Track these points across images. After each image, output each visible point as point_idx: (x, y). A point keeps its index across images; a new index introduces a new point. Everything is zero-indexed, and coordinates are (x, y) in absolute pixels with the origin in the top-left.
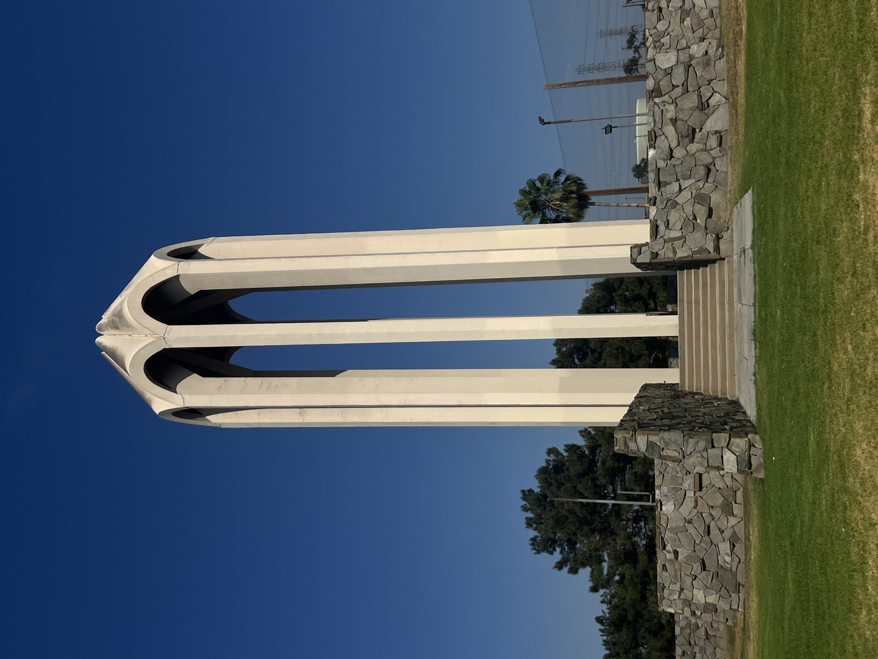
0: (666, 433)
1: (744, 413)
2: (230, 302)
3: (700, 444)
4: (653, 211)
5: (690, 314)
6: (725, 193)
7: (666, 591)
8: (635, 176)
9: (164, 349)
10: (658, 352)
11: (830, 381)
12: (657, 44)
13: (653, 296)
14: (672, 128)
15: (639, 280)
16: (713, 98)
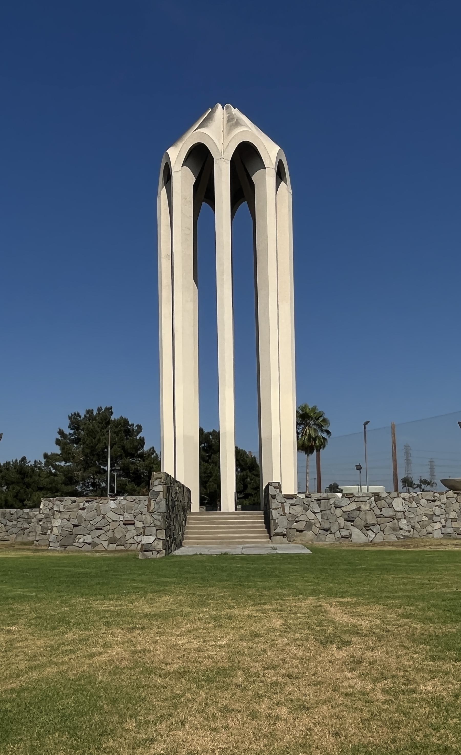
0: (165, 503)
1: (175, 550)
2: (246, 203)
3: (158, 522)
4: (302, 496)
5: (236, 518)
6: (312, 540)
7: (59, 503)
8: (331, 485)
9: (213, 158)
10: (211, 499)
11: (203, 587)
12: (412, 499)
13: (247, 496)
14: (354, 508)
15: (257, 488)
16: (372, 532)
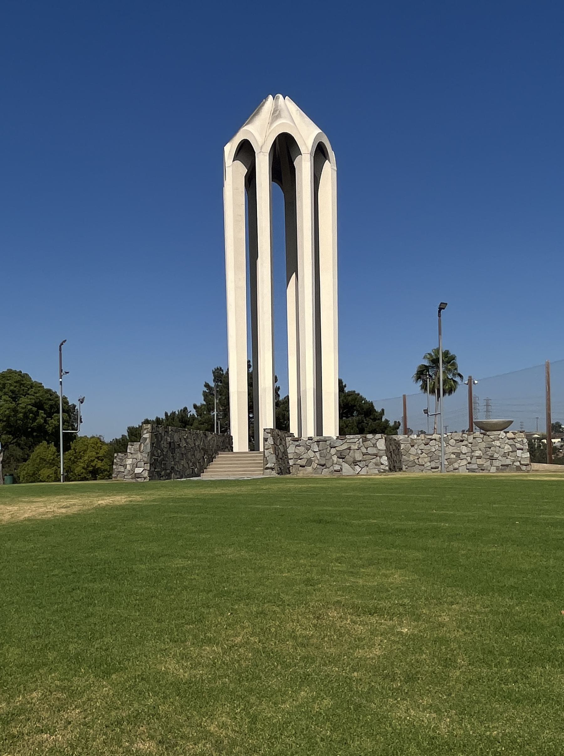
6: (312, 473)
